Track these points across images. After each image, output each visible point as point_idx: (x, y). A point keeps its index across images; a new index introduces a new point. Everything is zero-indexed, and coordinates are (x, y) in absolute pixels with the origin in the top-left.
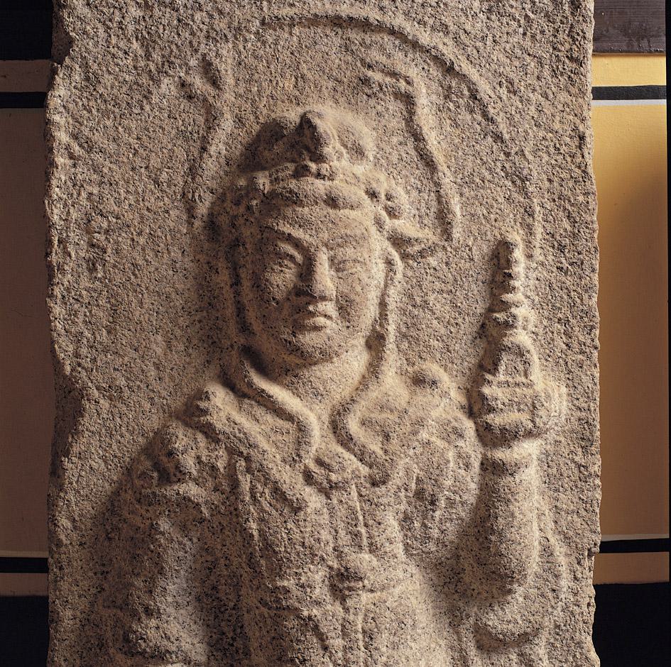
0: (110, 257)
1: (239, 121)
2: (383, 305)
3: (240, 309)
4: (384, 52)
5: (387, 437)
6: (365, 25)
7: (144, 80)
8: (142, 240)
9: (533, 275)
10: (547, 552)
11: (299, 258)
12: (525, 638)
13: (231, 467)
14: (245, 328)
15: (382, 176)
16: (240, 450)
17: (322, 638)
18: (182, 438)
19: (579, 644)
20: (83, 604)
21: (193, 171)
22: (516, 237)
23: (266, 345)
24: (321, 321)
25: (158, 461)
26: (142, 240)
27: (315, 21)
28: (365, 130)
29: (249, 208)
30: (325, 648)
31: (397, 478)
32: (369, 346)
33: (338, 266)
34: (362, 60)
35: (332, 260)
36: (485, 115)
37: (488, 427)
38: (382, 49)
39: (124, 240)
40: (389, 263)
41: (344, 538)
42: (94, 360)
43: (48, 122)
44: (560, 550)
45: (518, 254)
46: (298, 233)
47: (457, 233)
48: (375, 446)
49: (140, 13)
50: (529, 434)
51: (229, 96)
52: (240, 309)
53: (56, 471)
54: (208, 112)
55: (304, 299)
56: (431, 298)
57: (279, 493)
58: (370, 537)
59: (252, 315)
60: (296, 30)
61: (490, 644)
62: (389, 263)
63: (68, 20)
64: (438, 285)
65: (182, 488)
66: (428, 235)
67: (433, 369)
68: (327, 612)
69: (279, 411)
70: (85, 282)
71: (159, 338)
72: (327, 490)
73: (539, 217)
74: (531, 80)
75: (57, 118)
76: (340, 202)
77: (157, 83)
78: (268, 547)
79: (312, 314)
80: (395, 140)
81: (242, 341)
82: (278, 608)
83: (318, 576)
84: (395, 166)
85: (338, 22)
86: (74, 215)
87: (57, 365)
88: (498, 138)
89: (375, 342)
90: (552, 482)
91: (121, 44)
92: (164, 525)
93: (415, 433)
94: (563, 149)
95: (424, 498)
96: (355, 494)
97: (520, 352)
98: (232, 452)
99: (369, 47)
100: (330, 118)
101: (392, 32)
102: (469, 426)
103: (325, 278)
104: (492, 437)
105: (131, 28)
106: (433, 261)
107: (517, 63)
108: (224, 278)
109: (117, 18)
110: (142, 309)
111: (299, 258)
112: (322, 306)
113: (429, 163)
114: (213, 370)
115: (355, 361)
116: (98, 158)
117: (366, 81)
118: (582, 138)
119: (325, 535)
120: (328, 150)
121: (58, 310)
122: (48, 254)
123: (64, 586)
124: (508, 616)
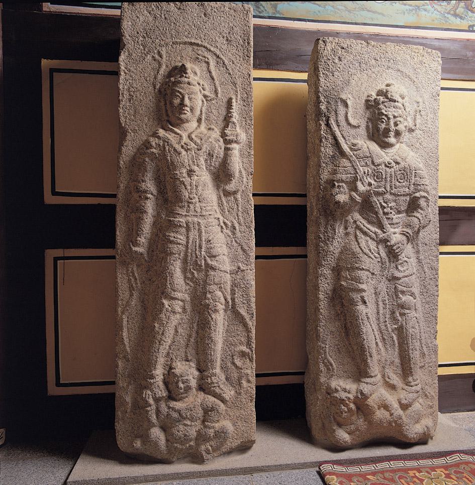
0: (135, 98)
1: (167, 66)
2: (201, 111)
3: (167, 111)
4: (201, 51)
5: (201, 139)
6: (198, 45)
7: (143, 55)
8: (142, 94)
9: (237, 106)
10: (240, 172)
11: (181, 97)
12: (235, 193)
13: (164, 145)
14: (167, 115)
15: (201, 81)
16: (166, 141)
17: (185, 186)
18: (151, 139)
19: (248, 195)
20: (126, 182)
21: (155, 78)
22: (234, 97)
23: (173, 119)
24: (186, 112)
25: (147, 145)
26: (142, 94)
27: (185, 43)
28: (197, 69)
29: (169, 85)
30: (186, 188)
31: (204, 149)
32: (198, 121)
33: (190, 99)
34: (197, 53)
35: (189, 97)
36: (226, 68)
37: (226, 139)
38: (202, 51)
39: (138, 94)
40: (203, 101)
41: (191, 162)
42: (130, 123)
43: (119, 64)
44: (244, 172)
45: (234, 101)
46: (181, 90)
47: (219, 95)
48: (198, 141)
49: (142, 39)
50: (236, 142)
51: (164, 60)
52: (167, 111)
53: (120, 150)
54: (159, 64)
55: (182, 106)
56: (213, 111)
57: (175, 150)
58: (197, 163)
59: (169, 112)
60: (181, 45)
61: (227, 194)
62: (203, 101)
63: (124, 40)
64: (215, 108)
65: (152, 150)
66: (213, 96)
67: (213, 127)
68: (187, 180)
69: (176, 133)
70: (128, 104)
71: (147, 118)
72: (187, 150)
73: (239, 93)
74: (238, 61)
75: (121, 63)
76: (191, 84)
77: (147, 56)
78: (172, 162)
79: (184, 110)
80: (205, 73)
81: (167, 119)
82: (175, 178)
83: (184, 171)
84: (204, 79)
85: (191, 44)
86: (126, 87)
87: (120, 124)
88: (230, 74)
89: (199, 121)
90: (242, 155)
91: (138, 46)
92: (147, 159)
93: (208, 139)
94: (245, 77)
95: (210, 155)
96: (193, 152)
97: (234, 123)
98: (164, 141)
99: (198, 50)
100: (188, 65)
101: (204, 47)
102: (221, 140)
103: (187, 101)
104: (227, 142)
105: (140, 43)
106: (213, 102)
107: (234, 57)
108: (163, 103)
109: (137, 40)
110: (142, 110)
111: (181, 97)
112: (186, 108)
113: (213, 79)
114: (160, 126)
115: (194, 124)
116: (132, 74)
117: (198, 58)
118: (250, 75)
119: (186, 161)
120: (188, 71)
121: (121, 110)
122: (119, 97)
123: (121, 178)
124: (231, 187)
